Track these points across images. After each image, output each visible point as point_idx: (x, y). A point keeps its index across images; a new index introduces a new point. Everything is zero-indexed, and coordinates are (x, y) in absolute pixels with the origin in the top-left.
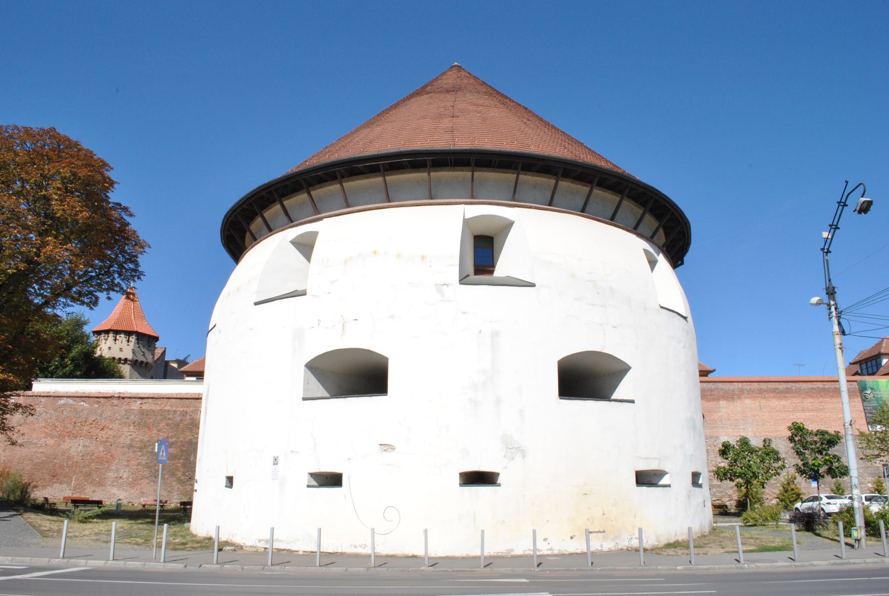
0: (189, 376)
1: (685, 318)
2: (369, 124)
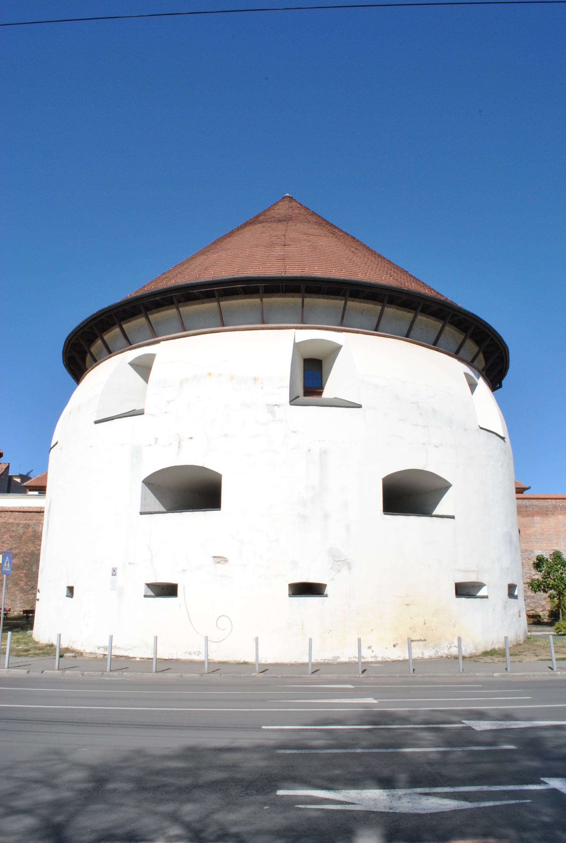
1: (503, 438)
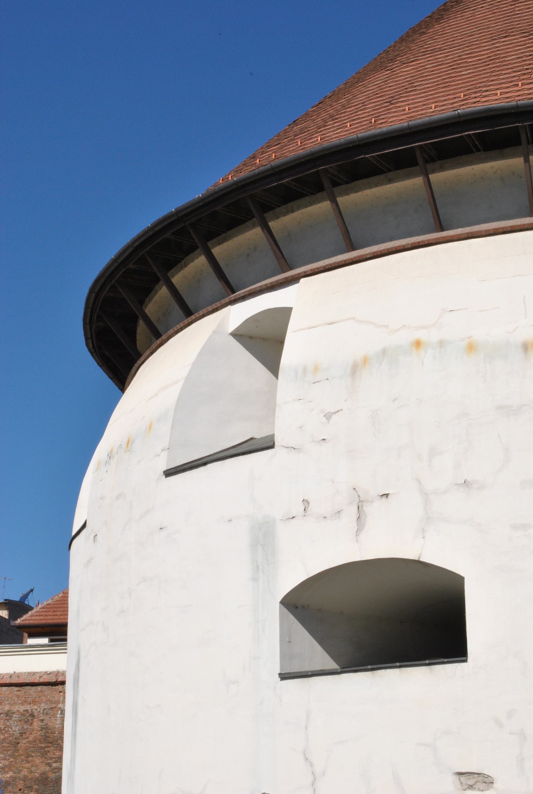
0: (32, 635)
2: (384, 61)
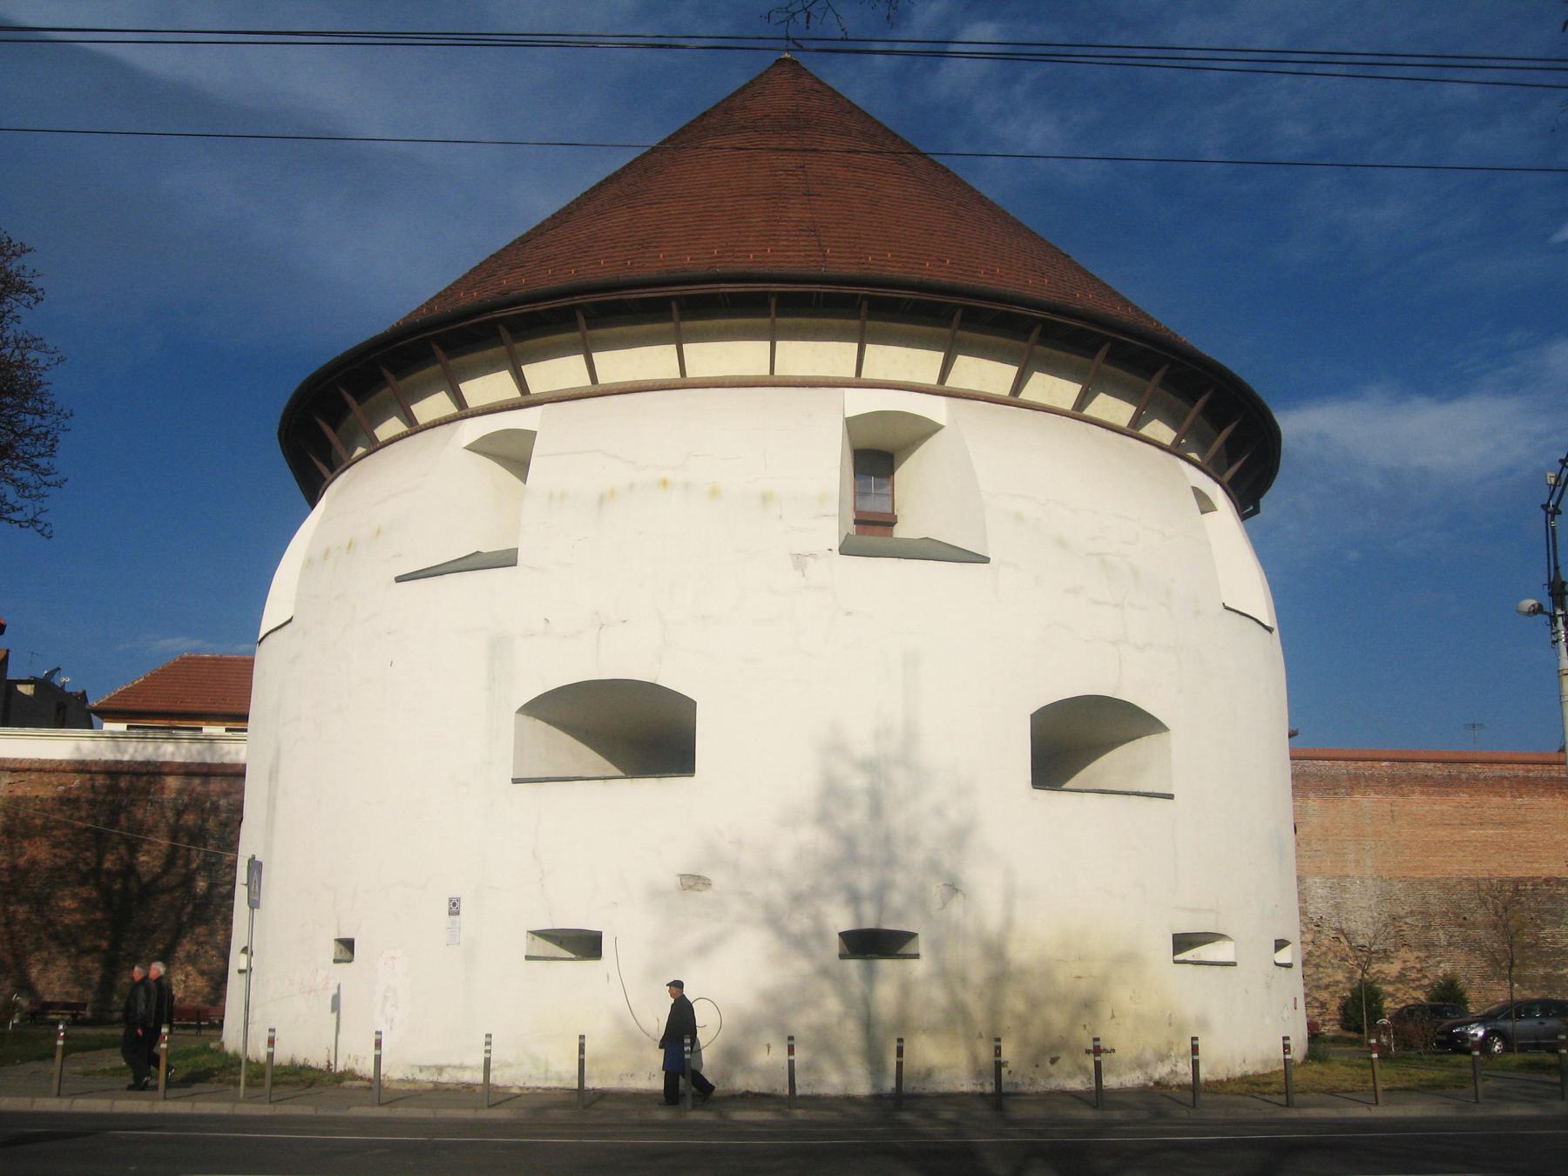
1: (1270, 630)
